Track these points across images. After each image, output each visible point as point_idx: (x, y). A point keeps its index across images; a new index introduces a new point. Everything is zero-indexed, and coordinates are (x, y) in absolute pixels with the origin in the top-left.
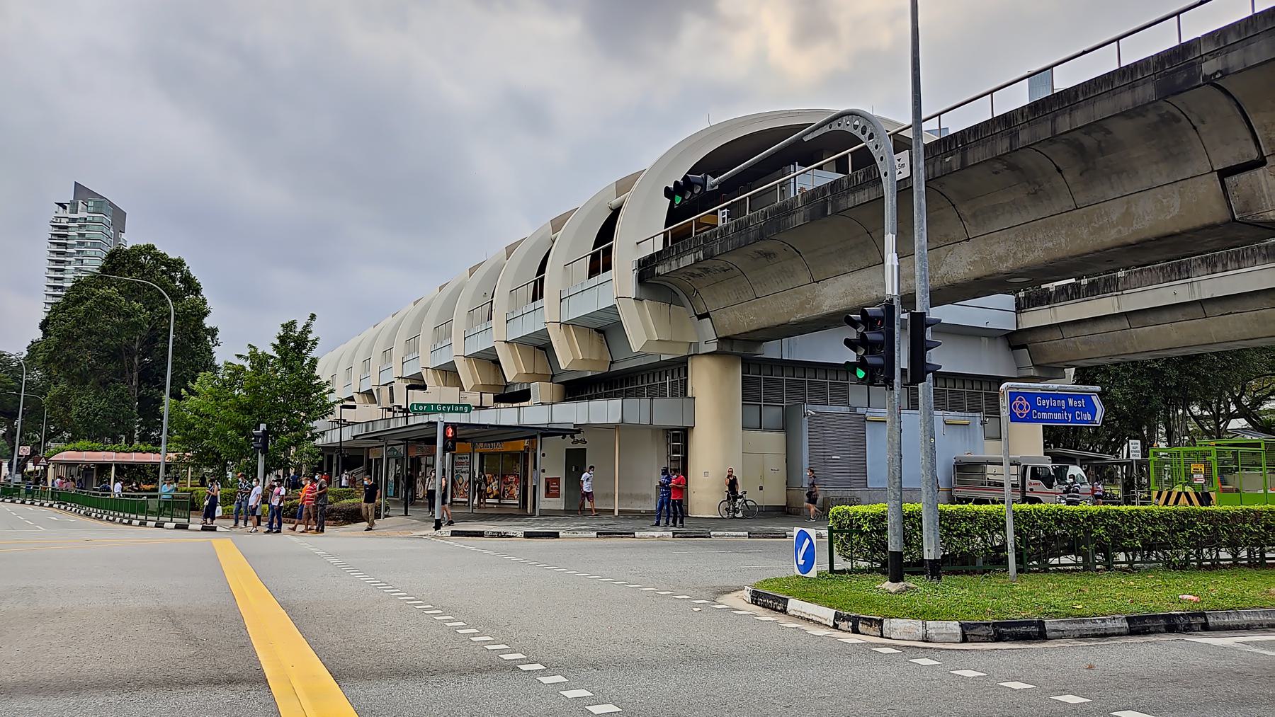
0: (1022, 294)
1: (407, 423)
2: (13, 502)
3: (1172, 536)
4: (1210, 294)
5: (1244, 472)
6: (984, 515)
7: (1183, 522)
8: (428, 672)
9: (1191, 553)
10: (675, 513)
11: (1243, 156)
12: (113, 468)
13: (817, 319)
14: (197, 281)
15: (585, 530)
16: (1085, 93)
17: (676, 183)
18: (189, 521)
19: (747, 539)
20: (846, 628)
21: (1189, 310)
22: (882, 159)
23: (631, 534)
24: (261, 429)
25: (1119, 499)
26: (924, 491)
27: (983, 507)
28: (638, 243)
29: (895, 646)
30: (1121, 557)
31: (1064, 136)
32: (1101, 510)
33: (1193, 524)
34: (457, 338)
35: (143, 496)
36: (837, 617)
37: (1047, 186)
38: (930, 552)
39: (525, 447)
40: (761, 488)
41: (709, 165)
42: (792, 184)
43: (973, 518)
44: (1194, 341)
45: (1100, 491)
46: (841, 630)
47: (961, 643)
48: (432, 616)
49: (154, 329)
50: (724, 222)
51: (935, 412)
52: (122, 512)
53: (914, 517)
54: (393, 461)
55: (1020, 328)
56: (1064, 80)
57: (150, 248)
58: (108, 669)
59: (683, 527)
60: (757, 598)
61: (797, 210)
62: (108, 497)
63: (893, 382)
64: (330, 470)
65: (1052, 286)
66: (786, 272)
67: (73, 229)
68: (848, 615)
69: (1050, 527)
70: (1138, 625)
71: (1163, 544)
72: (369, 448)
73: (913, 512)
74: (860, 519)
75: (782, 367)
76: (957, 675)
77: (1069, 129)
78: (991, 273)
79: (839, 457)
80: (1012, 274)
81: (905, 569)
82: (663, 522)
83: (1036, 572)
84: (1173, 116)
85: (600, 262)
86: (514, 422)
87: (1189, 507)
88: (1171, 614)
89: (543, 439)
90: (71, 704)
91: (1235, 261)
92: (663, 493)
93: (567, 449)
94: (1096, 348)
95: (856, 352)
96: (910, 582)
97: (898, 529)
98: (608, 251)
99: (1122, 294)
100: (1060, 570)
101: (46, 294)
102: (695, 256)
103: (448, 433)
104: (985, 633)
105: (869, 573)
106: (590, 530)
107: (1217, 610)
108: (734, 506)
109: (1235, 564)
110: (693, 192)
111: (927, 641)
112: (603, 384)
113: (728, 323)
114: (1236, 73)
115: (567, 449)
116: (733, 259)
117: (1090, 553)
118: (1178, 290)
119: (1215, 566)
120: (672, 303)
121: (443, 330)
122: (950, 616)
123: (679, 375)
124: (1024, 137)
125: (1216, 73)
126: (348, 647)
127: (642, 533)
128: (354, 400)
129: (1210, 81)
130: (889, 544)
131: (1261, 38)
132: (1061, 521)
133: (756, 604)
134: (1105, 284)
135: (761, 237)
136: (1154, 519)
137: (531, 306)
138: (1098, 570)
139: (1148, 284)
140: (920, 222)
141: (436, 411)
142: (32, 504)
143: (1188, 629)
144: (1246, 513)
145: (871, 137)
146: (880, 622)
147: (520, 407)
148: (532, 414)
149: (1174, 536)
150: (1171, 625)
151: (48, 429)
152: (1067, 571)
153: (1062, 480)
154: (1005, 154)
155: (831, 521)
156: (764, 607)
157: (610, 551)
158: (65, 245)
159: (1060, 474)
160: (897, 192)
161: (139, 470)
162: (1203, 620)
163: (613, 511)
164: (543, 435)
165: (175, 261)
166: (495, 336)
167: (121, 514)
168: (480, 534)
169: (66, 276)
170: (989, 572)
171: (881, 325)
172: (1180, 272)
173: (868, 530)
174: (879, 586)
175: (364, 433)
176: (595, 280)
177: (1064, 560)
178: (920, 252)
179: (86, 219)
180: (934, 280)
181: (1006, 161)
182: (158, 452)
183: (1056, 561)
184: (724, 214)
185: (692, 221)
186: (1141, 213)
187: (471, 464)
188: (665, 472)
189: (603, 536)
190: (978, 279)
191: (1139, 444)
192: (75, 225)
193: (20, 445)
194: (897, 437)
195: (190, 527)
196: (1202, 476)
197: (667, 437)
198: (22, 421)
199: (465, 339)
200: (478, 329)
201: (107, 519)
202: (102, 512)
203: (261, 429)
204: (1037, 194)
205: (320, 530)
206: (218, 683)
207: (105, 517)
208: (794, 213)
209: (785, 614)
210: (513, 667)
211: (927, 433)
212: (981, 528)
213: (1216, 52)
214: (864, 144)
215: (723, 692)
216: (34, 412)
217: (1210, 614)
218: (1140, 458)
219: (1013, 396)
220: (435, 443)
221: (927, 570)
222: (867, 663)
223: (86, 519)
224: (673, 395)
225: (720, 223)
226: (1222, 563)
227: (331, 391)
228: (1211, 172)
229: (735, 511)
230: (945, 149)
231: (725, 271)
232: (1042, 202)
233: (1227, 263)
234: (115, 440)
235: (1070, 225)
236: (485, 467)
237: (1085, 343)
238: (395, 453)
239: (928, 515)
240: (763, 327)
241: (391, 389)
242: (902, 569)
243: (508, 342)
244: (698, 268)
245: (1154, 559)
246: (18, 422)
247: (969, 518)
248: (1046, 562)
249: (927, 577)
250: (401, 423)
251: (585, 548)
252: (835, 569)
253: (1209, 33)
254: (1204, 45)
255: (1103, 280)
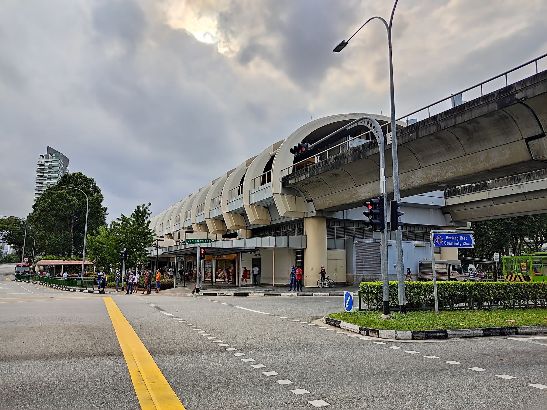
0: (447, 191)
1: (185, 247)
2: (21, 281)
3: (507, 295)
4: (528, 190)
5: (545, 267)
6: (425, 286)
7: (512, 288)
8: (189, 351)
9: (516, 302)
10: (298, 285)
11: (535, 133)
12: (62, 267)
13: (358, 202)
14: (99, 188)
15: (260, 293)
16: (468, 107)
17: (295, 147)
18: (94, 289)
19: (329, 296)
20: (364, 334)
21: (519, 197)
22: (378, 137)
23: (279, 294)
24: (124, 250)
25: (492, 279)
26: (399, 276)
27: (425, 283)
28: (282, 171)
29: (383, 341)
30: (485, 303)
31: (459, 125)
32: (476, 284)
33: (516, 290)
34: (206, 211)
35: (66, 279)
36: (360, 329)
37: (453, 146)
38: (402, 301)
39: (235, 257)
40: (336, 275)
41: (308, 140)
42: (348, 145)
43: (421, 287)
44: (522, 210)
45: (483, 275)
46: (362, 334)
47: (412, 340)
48: (192, 329)
49: (80, 208)
50: (317, 161)
51: (403, 241)
52: (66, 285)
53: (395, 287)
54: (179, 263)
55: (447, 205)
56: (466, 98)
57: (81, 174)
58: (59, 350)
59: (301, 291)
60: (328, 321)
61: (348, 156)
62: (60, 279)
63: (384, 230)
64: (153, 267)
65: (460, 187)
66: (344, 182)
67: (47, 166)
68: (365, 328)
69: (454, 291)
70: (487, 332)
71: (503, 298)
72: (170, 258)
73: (394, 285)
74: (372, 288)
75: (344, 222)
76: (407, 353)
77: (461, 122)
78: (430, 182)
79: (369, 261)
80: (439, 183)
81: (391, 309)
82: (293, 289)
83: (449, 310)
84: (506, 116)
85: (266, 179)
86: (230, 247)
87: (521, 283)
88: (502, 328)
89: (242, 253)
90: (44, 364)
91: (538, 176)
92: (293, 277)
93: (253, 258)
94: (480, 213)
95: (369, 217)
96: (392, 314)
97: (387, 291)
98: (269, 174)
99: (490, 190)
100: (459, 310)
101: (35, 193)
102: (306, 176)
103: (202, 252)
104: (421, 336)
105: (376, 311)
106: (262, 293)
107: (522, 326)
108: (324, 282)
109: (536, 306)
110: (302, 151)
111: (397, 339)
112: (268, 230)
113: (320, 204)
114: (530, 98)
115: (253, 258)
116: (321, 177)
117: (472, 302)
118: (514, 188)
119: (527, 307)
120: (296, 196)
121: (201, 208)
122: (408, 329)
123: (300, 226)
124: (443, 125)
125: (522, 98)
126: (157, 341)
127: (284, 294)
128: (163, 238)
129: (519, 101)
130: (383, 298)
131: (541, 83)
132: (459, 288)
133: (328, 324)
134: (483, 186)
135: (333, 168)
136: (499, 287)
137: (238, 197)
138: (475, 309)
139: (501, 186)
140: (395, 163)
141: (197, 242)
142: (29, 282)
143: (509, 334)
144: (539, 285)
145: (374, 128)
146: (378, 331)
147: (232, 240)
148: (238, 243)
149: (508, 294)
150: (502, 332)
151: (35, 250)
152: (462, 310)
153: (466, 270)
154: (435, 132)
155: (360, 289)
156: (331, 325)
157: (269, 301)
158: (43, 172)
159: (465, 268)
160: (385, 150)
161: (73, 268)
162: (516, 330)
163: (272, 284)
164: (242, 252)
165: (90, 179)
166: (223, 210)
167: (66, 287)
168: (215, 294)
169: (43, 186)
170: (428, 310)
171: (378, 206)
172: (515, 180)
173: (376, 292)
174: (379, 316)
175: (167, 251)
176: (265, 186)
177: (460, 305)
178: (395, 175)
179: (52, 162)
180: (407, 186)
181: (435, 135)
182: (81, 260)
183: (457, 306)
184: (317, 158)
185: (304, 161)
186: (493, 156)
187: (212, 265)
188: (293, 268)
189: (267, 295)
190: (425, 185)
191: (498, 255)
192: (47, 164)
193: (24, 258)
194: (386, 253)
195: (94, 292)
196: (526, 268)
197: (295, 252)
198: (25, 247)
199: (210, 211)
200: (215, 207)
201: (60, 289)
202: (58, 286)
203: (124, 250)
204: (449, 149)
205: (149, 293)
206: (103, 355)
207: (59, 288)
208: (347, 158)
209: (340, 328)
210: (224, 350)
211: (399, 251)
212: (424, 291)
213: (522, 90)
214: (371, 131)
215: (309, 360)
216: (30, 242)
217: (519, 328)
218: (499, 261)
219: (436, 235)
220: (196, 256)
221: (400, 309)
222: (371, 348)
223: (51, 289)
224: (297, 235)
225: (316, 162)
226: (530, 306)
227: (155, 235)
228: (522, 139)
229: (324, 284)
230: (410, 130)
231: (318, 182)
232: (451, 152)
233: (535, 177)
234: (63, 255)
235: (464, 162)
236: (218, 266)
237: (475, 211)
238: (181, 260)
239: (400, 286)
240: (335, 205)
241: (179, 233)
242: (389, 309)
243: (228, 213)
244: (307, 181)
245: (500, 304)
246: (23, 247)
247: (418, 287)
248: (453, 306)
249: (400, 312)
250: (183, 247)
251: (259, 300)
252: (361, 309)
253: (519, 82)
254: (517, 87)
255: (482, 184)
